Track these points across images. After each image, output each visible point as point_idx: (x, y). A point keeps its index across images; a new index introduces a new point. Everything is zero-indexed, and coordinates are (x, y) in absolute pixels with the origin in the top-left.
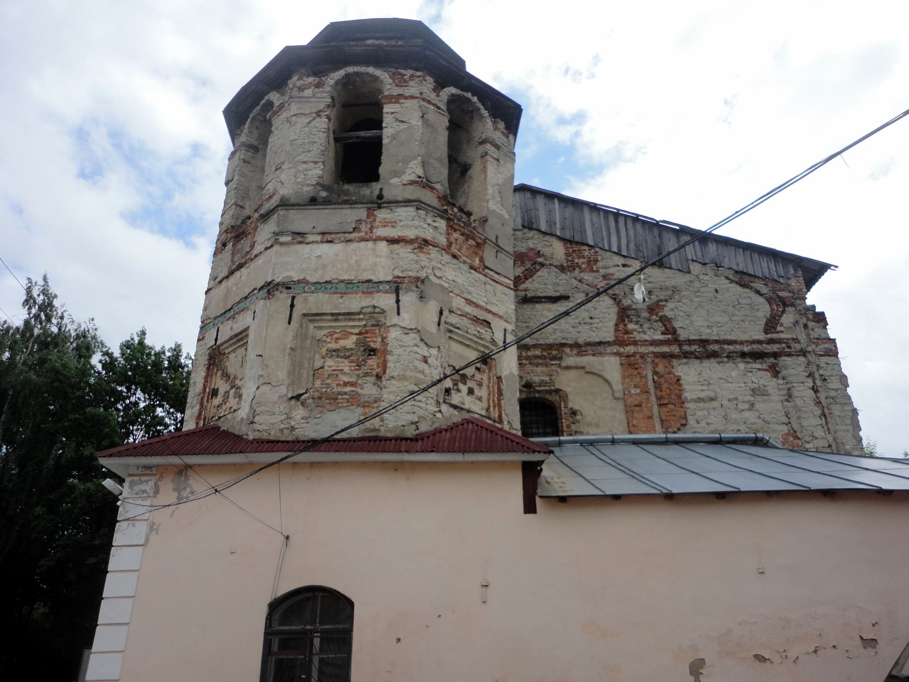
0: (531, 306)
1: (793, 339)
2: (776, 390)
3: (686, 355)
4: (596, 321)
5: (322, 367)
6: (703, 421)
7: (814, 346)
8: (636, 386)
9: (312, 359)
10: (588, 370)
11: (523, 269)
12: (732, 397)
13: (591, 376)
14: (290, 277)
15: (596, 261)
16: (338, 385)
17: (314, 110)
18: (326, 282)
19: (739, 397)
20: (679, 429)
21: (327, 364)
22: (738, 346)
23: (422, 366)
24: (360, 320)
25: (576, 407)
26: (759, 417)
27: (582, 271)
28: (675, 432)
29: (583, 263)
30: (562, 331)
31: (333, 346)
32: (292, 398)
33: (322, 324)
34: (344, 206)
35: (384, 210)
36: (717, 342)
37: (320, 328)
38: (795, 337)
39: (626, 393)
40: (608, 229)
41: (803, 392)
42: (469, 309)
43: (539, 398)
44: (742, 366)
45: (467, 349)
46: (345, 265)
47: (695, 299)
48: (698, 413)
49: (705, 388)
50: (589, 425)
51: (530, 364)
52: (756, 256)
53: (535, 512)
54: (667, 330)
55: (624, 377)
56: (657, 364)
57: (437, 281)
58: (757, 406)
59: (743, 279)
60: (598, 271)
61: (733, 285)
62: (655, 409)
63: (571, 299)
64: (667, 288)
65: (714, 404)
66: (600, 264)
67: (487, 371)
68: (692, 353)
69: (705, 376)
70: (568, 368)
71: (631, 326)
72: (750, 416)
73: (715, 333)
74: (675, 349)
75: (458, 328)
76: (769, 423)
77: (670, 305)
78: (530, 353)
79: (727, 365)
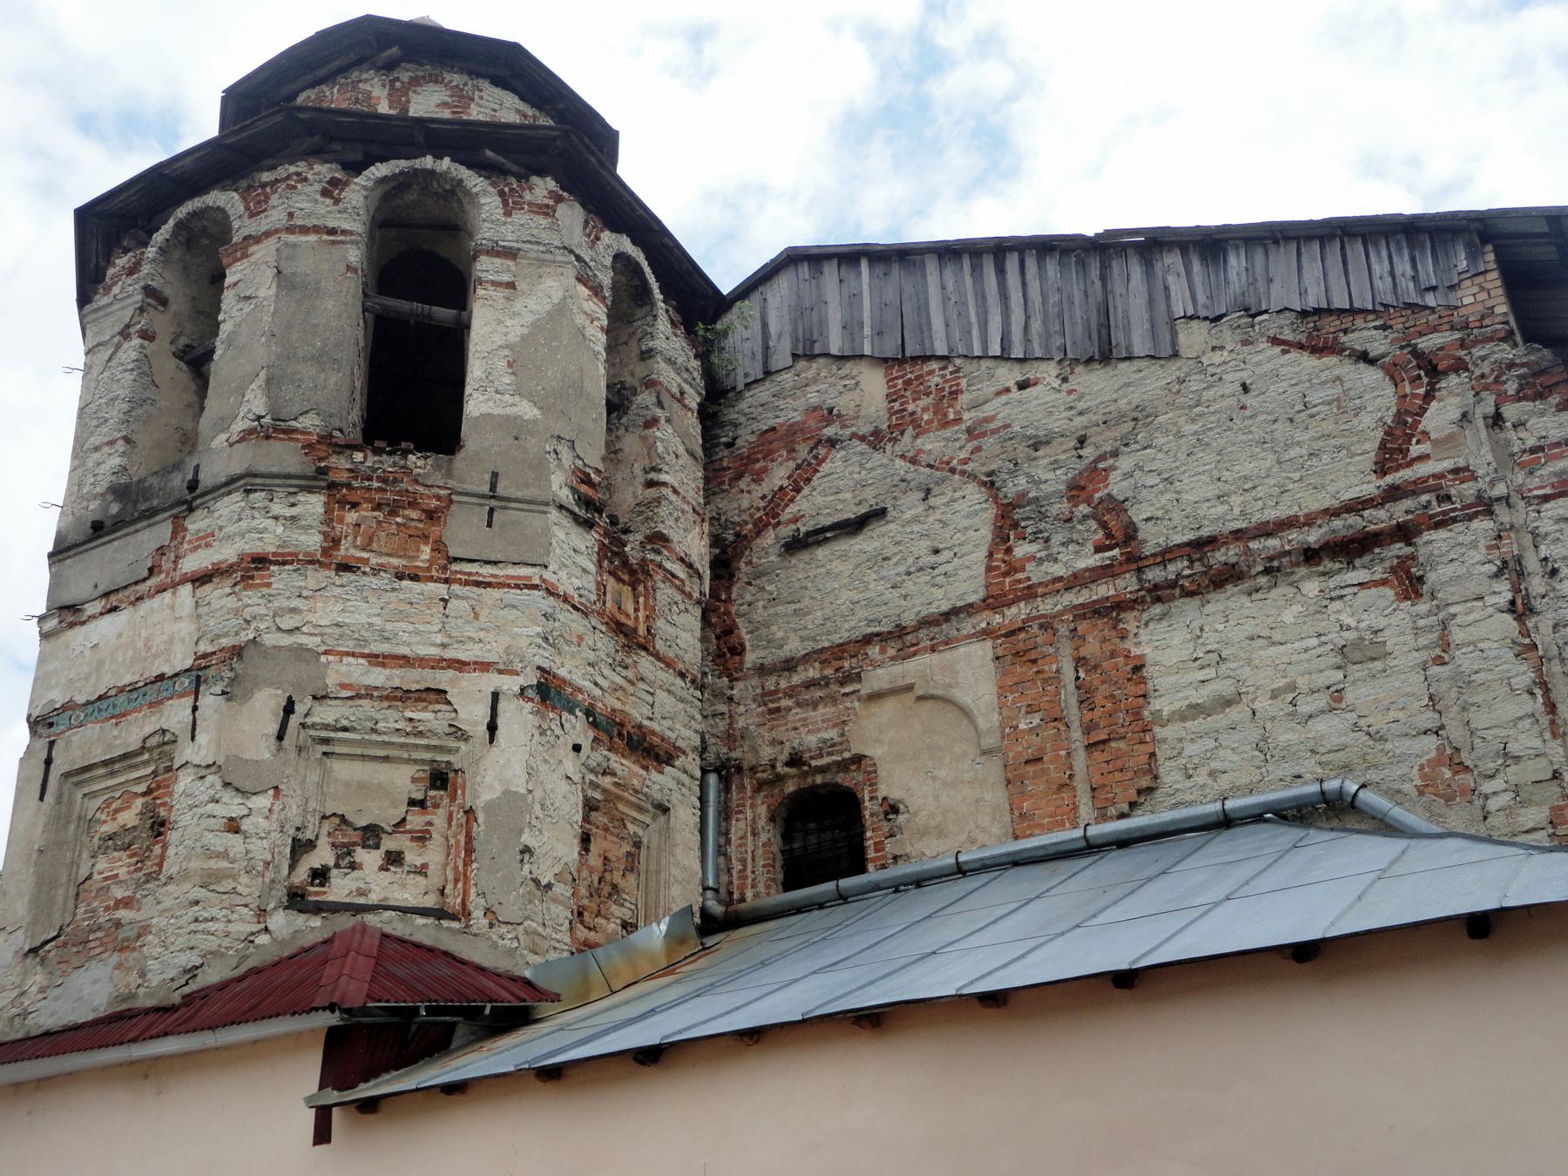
0: (805, 556)
1: (1456, 471)
2: (1409, 638)
3: (1158, 594)
4: (946, 555)
5: (89, 878)
6: (1202, 766)
7: (1520, 477)
8: (1031, 710)
9: (74, 864)
10: (919, 692)
11: (792, 465)
12: (1281, 683)
13: (928, 705)
14: (52, 701)
15: (955, 394)
16: (107, 908)
17: (117, 329)
18: (100, 698)
19: (1302, 682)
20: (1133, 805)
21: (99, 867)
22: (1293, 535)
23: (235, 843)
24: (145, 763)
25: (895, 794)
26: (1356, 728)
27: (920, 430)
28: (1122, 816)
29: (925, 410)
30: (869, 603)
31: (108, 828)
32: (31, 951)
33: (96, 787)
34: (139, 526)
35: (198, 513)
36: (1238, 535)
37: (92, 795)
38: (1461, 463)
39: (1010, 731)
40: (981, 298)
41: (1485, 628)
42: (379, 677)
43: (825, 785)
44: (1312, 587)
45: (385, 766)
46: (130, 653)
47: (1189, 428)
48: (1190, 749)
49: (1209, 673)
50: (924, 832)
51: (799, 705)
52: (1356, 250)
53: (315, 1143)
54: (1109, 536)
55: (1002, 691)
56: (1083, 638)
57: (286, 640)
58: (1349, 697)
59: (1319, 331)
60: (958, 420)
61: (1294, 355)
62: (1080, 760)
63: (892, 513)
64: (1121, 417)
65: (1235, 714)
66: (964, 399)
67: (446, 801)
68: (1172, 585)
69: (1211, 640)
70: (876, 696)
71: (1021, 550)
72: (1331, 729)
73: (1237, 511)
74: (1127, 584)
75: (345, 729)
76: (1383, 739)
77: (1125, 463)
78: (796, 679)
79: (1274, 593)
